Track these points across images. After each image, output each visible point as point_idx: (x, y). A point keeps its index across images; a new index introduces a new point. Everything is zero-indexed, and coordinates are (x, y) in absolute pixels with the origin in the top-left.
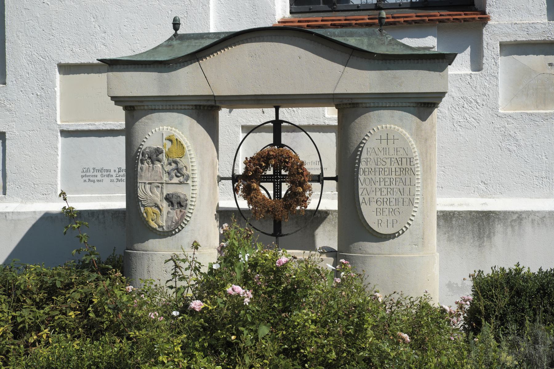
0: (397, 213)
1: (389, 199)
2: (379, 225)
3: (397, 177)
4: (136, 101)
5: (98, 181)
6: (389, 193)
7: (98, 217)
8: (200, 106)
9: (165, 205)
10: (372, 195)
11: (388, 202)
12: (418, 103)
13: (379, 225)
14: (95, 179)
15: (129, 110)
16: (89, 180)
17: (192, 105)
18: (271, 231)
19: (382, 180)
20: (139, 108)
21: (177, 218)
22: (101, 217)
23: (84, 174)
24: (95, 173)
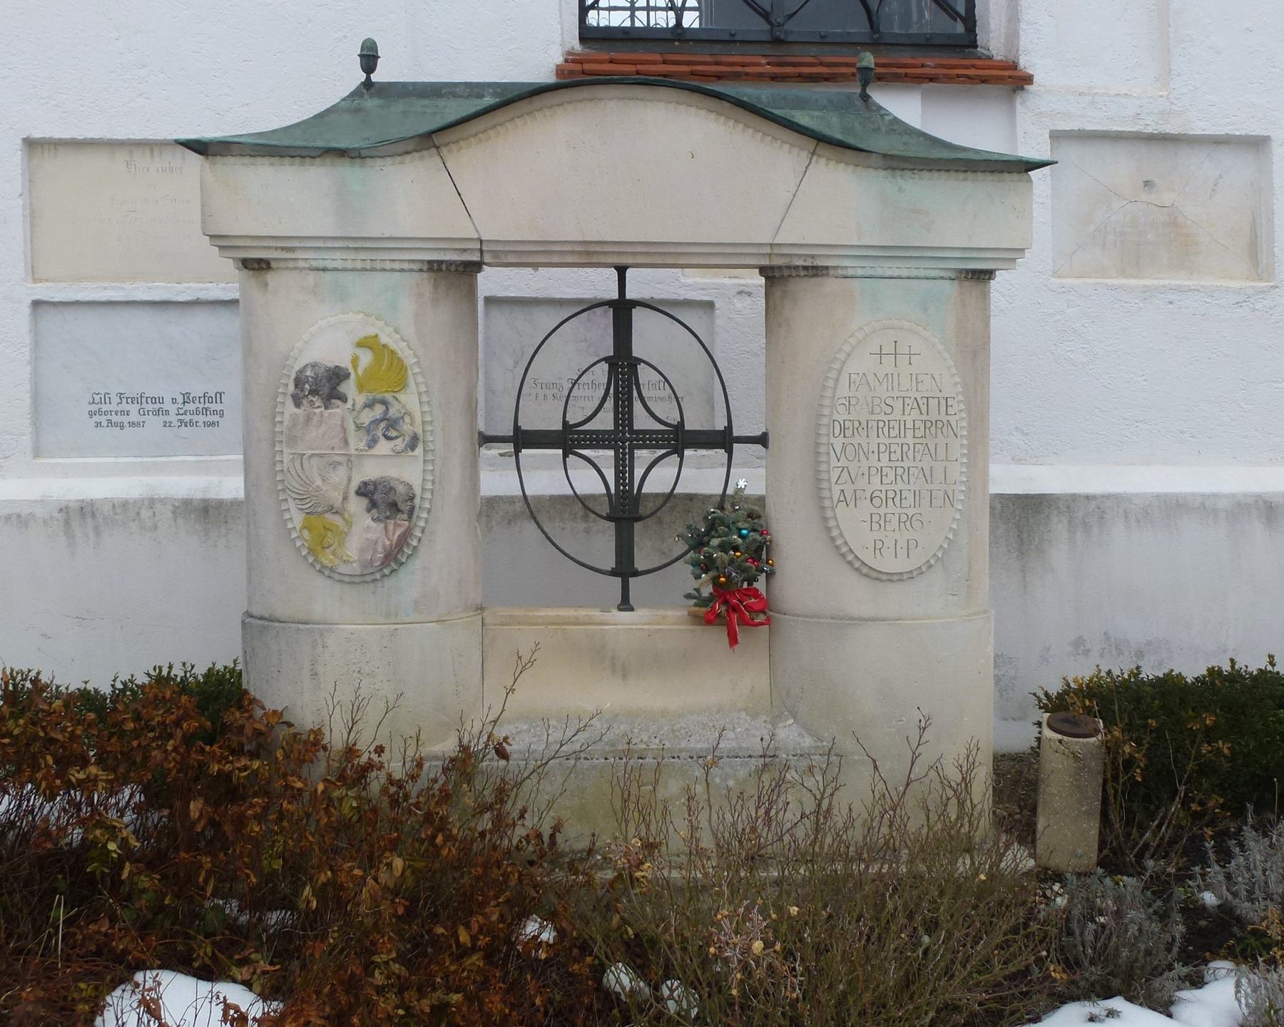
0: (916, 524)
1: (898, 493)
2: (877, 551)
3: (917, 441)
4: (276, 248)
5: (132, 424)
6: (898, 477)
7: (138, 514)
8: (440, 262)
9: (357, 506)
10: (862, 483)
11: (897, 500)
12: (961, 271)
13: (877, 551)
14: (125, 419)
15: (253, 269)
16: (109, 421)
17: (422, 261)
18: (609, 562)
19: (882, 448)
20: (282, 265)
21: (388, 543)
22: (145, 513)
23: (94, 408)
24: (124, 406)
